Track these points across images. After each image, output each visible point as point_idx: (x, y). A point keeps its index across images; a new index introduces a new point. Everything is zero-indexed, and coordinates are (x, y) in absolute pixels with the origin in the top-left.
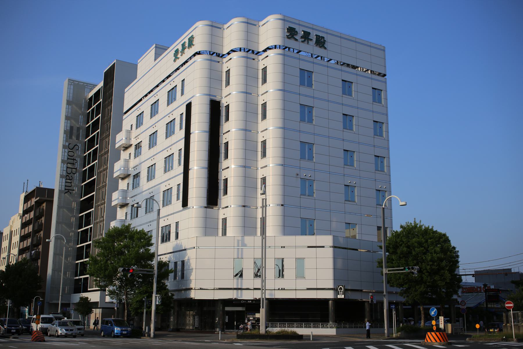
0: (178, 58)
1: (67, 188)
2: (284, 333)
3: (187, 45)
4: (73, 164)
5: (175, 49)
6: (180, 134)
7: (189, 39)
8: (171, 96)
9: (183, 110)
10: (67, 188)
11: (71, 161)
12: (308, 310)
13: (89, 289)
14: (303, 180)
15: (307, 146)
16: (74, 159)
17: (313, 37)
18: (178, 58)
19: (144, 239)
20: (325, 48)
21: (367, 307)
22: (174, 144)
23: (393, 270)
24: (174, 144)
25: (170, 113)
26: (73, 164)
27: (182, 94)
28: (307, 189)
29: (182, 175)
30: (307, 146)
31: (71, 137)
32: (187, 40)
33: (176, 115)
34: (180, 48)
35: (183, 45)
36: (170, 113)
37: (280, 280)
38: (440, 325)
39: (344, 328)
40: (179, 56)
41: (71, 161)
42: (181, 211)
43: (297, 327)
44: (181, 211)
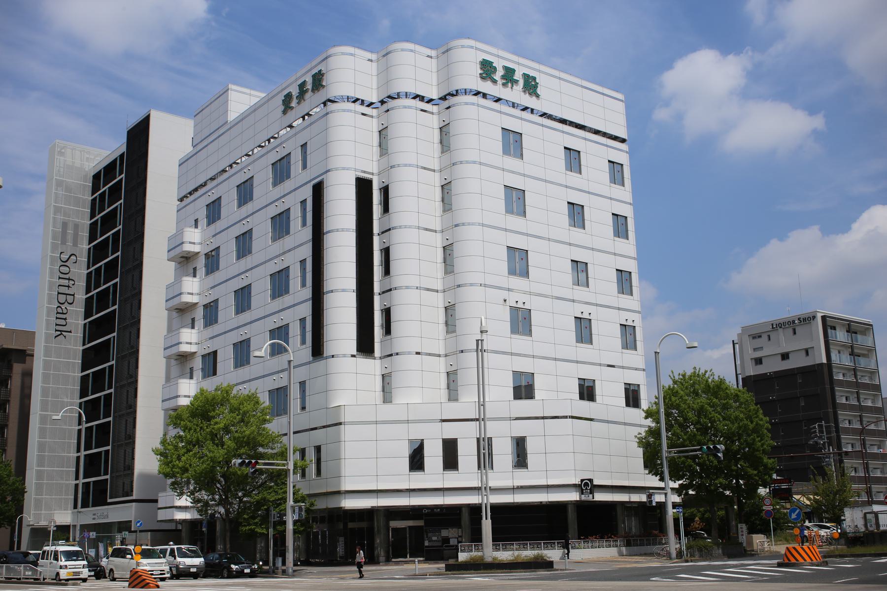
0: (292, 108)
1: (59, 328)
2: (540, 560)
3: (309, 86)
4: (69, 287)
5: (286, 92)
6: (301, 233)
7: (314, 76)
8: (281, 170)
9: (307, 193)
10: (59, 328)
11: (66, 282)
12: (589, 518)
13: (109, 501)
14: (514, 310)
15: (517, 254)
16: (69, 279)
17: (518, 76)
18: (292, 108)
19: (244, 410)
20: (538, 96)
21: (572, 515)
22: (289, 251)
23: (278, 465)
24: (289, 251)
25: (277, 200)
26: (69, 287)
27: (305, 167)
28: (520, 324)
29: (310, 303)
30: (517, 254)
31: (64, 242)
32: (309, 79)
33: (293, 203)
34: (295, 92)
35: (302, 86)
36: (277, 200)
37: (521, 472)
38: (740, 537)
39: (592, 547)
40: (293, 104)
41: (66, 282)
42: (309, 363)
43: (546, 548)
44: (309, 363)
